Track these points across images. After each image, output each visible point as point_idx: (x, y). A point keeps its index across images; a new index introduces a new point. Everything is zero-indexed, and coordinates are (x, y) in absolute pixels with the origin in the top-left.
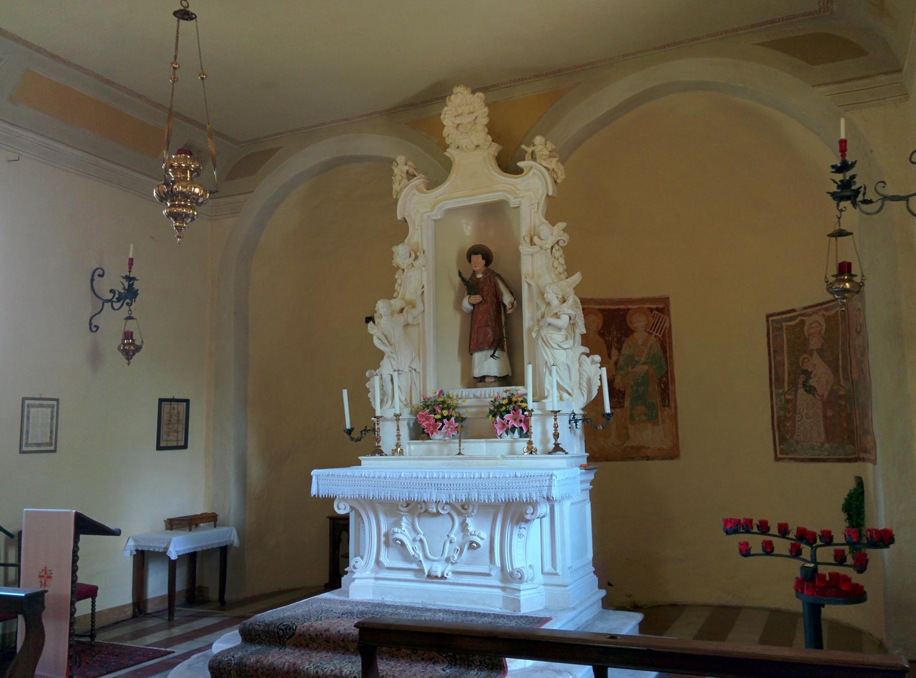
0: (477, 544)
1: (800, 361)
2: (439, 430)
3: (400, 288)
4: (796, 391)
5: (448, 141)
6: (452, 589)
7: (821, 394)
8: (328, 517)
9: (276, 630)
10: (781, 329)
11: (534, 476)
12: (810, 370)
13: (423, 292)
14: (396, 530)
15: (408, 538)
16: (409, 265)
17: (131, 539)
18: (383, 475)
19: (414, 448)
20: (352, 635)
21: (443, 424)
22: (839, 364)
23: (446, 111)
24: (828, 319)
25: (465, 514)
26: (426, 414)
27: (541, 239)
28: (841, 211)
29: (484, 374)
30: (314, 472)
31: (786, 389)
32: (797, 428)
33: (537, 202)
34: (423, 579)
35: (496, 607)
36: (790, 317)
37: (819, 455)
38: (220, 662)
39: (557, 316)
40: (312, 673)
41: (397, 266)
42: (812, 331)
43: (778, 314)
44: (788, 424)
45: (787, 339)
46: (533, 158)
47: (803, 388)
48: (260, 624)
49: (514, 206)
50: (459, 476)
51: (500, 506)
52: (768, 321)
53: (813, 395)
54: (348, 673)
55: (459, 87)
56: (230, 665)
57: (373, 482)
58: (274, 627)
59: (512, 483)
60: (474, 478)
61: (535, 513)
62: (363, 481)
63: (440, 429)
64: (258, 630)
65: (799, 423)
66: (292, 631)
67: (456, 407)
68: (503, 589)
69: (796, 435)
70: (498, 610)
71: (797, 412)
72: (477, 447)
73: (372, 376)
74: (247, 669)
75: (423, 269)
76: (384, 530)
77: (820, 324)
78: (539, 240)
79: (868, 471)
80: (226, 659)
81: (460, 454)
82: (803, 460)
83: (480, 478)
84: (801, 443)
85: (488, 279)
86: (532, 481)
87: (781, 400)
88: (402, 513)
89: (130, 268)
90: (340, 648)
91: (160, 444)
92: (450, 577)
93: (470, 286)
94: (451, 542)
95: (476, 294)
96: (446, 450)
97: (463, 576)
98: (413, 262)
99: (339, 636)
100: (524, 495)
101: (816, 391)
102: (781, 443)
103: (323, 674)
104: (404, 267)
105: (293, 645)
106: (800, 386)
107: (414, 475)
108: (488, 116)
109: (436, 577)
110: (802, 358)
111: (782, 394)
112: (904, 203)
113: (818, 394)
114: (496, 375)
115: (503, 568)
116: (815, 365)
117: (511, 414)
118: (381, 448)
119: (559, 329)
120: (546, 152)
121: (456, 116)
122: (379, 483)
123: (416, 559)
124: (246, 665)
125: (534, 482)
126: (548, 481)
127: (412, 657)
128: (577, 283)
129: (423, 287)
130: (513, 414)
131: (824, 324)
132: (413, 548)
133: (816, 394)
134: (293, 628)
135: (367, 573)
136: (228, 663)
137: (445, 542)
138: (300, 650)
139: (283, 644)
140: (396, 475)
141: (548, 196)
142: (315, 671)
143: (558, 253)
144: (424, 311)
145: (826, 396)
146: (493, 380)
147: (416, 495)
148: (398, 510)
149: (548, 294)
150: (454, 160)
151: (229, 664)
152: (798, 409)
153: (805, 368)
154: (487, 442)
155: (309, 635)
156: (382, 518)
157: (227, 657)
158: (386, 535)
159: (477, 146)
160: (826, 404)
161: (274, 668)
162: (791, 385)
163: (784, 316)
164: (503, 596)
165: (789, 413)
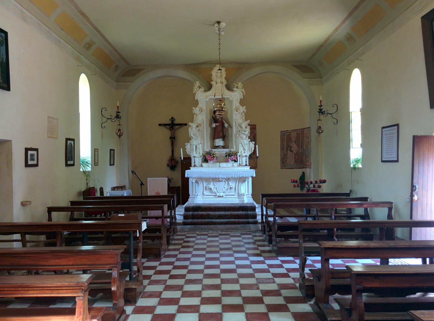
0: (232, 188)
4: (288, 151)
5: (213, 79)
12: (292, 146)
14: (209, 185)
17: (108, 193)
18: (208, 171)
19: (204, 165)
21: (213, 159)
24: (297, 134)
28: (320, 115)
30: (186, 171)
31: (285, 150)
36: (287, 132)
39: (245, 131)
46: (237, 88)
52: (281, 133)
63: (213, 160)
67: (216, 154)
68: (238, 198)
72: (223, 165)
73: (187, 145)
74: (195, 216)
76: (205, 186)
79: (307, 171)
81: (220, 166)
87: (283, 153)
89: (118, 109)
91: (395, 161)
92: (224, 196)
93: (215, 120)
94: (225, 188)
96: (214, 166)
102: (283, 164)
104: (197, 114)
106: (289, 150)
107: (217, 171)
109: (221, 197)
112: (331, 115)
114: (223, 145)
115: (238, 193)
116: (293, 145)
119: (245, 134)
120: (241, 87)
129: (203, 120)
131: (296, 135)
135: (200, 197)
141: (241, 98)
143: (244, 114)
144: (204, 127)
148: (210, 180)
150: (213, 84)
153: (290, 145)
154: (226, 163)
156: (204, 183)
158: (206, 187)
163: (286, 132)
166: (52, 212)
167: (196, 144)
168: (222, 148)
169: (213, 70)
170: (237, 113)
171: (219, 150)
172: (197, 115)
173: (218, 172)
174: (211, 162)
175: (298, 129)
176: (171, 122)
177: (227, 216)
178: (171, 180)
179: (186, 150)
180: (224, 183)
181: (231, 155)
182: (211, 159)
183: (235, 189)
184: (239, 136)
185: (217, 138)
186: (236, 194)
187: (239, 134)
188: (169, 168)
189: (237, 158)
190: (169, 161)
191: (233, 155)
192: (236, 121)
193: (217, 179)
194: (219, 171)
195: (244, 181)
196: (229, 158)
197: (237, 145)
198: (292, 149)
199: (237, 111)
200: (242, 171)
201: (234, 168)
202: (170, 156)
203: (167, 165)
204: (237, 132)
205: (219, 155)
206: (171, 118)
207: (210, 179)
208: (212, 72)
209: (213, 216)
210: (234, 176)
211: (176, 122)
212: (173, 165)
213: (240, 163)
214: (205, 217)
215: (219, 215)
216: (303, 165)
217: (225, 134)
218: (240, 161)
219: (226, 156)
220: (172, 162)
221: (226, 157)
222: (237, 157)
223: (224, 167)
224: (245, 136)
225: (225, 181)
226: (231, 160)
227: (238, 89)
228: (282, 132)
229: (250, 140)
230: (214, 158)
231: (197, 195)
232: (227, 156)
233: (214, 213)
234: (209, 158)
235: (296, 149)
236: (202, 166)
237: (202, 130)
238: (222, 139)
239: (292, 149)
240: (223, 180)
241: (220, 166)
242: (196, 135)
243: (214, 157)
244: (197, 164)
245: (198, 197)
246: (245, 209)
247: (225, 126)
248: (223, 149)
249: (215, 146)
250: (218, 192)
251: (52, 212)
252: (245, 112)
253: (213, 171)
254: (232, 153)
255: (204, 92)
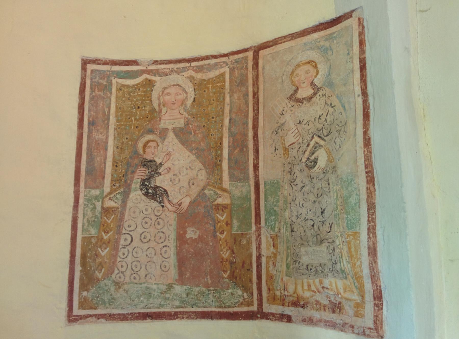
1: (140, 145)
4: (126, 195)
7: (175, 201)
10: (107, 88)
12: (158, 161)
22: (221, 155)
31: (107, 189)
32: (119, 259)
37: (161, 306)
42: (167, 98)
44: (104, 252)
52: (84, 69)
65: (125, 251)
69: (116, 271)
71: (124, 231)
77: (184, 91)
82: (124, 318)
84: (126, 287)
87: (95, 208)
102: (83, 287)
106: (136, 184)
111: (96, 198)
116: (169, 154)
145: (185, 205)
152: (126, 225)
153: (149, 157)
162: (117, 185)
166: (264, 311)
175: (207, 58)
198: (158, 181)
216: (246, 289)
235: (191, 183)
239: (158, 181)
251: (264, 311)
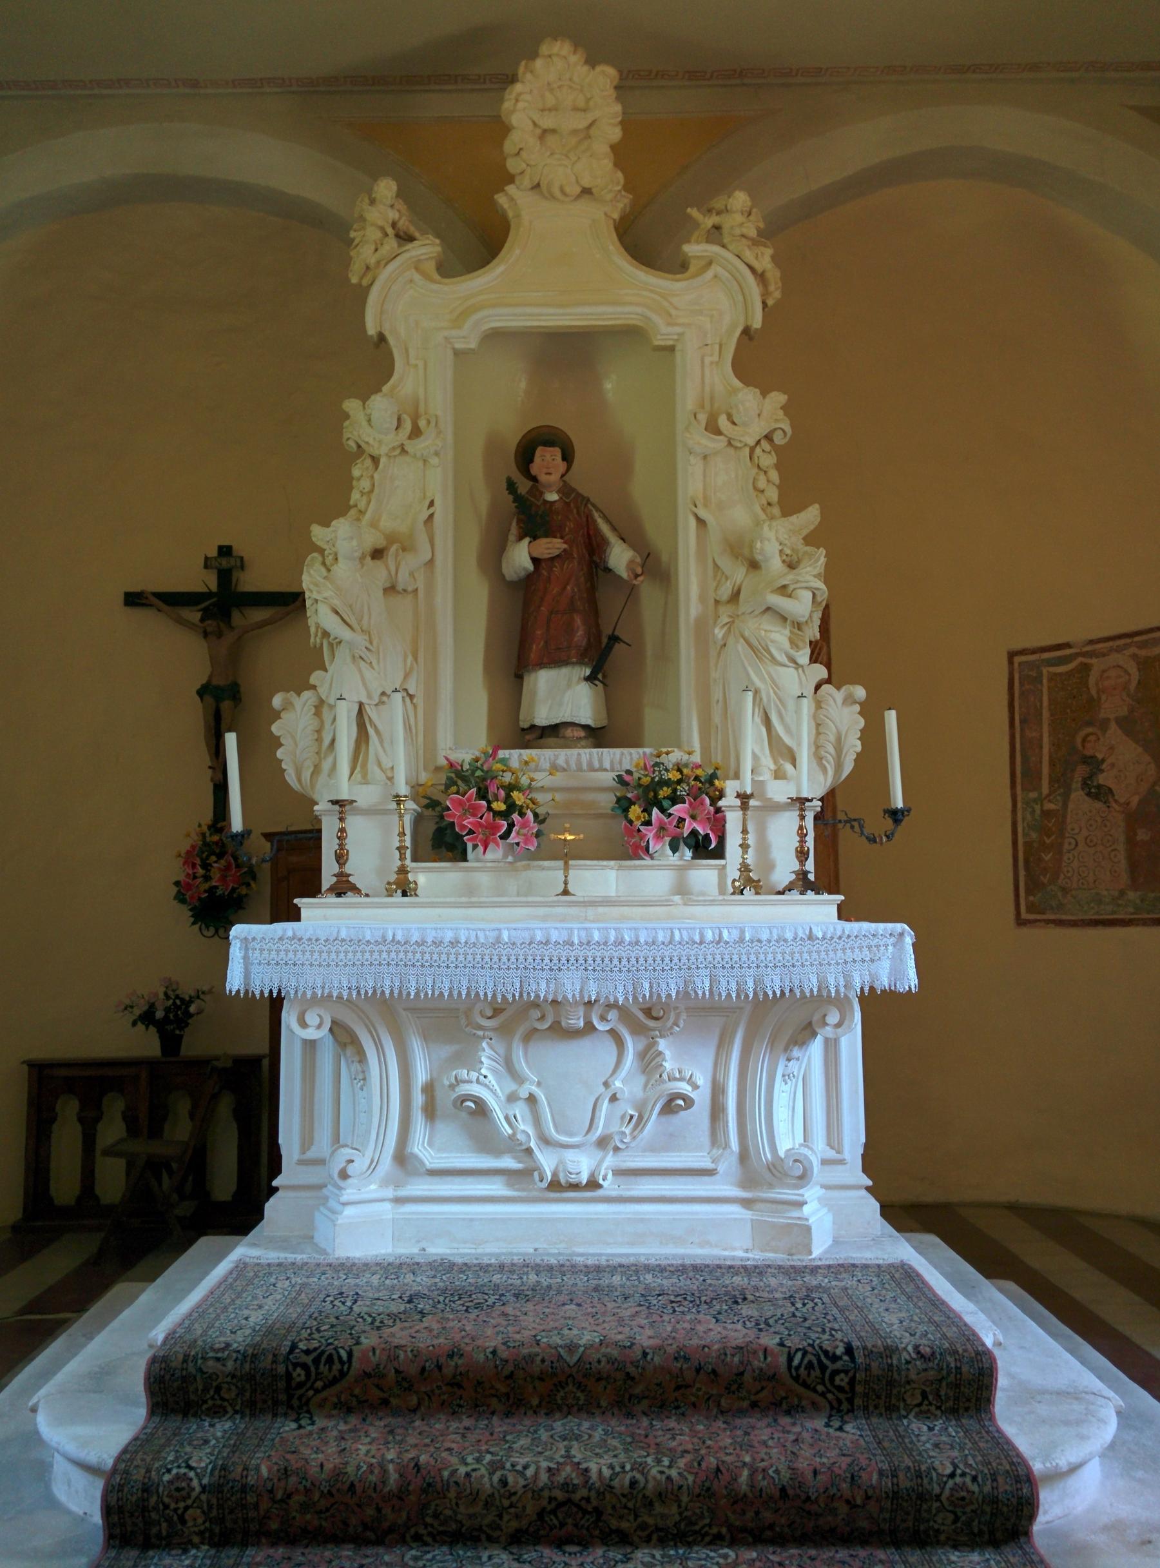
0: (684, 1098)
1: (1079, 740)
2: (501, 837)
3: (369, 502)
5: (512, 165)
6: (619, 1213)
7: (1122, 800)
8: (24, 1062)
9: (281, 1369)
11: (856, 937)
12: (1100, 756)
13: (431, 516)
14: (463, 1073)
15: (495, 1094)
16: (394, 449)
18: (449, 936)
20: (539, 1359)
21: (511, 826)
23: (519, 94)
25: (653, 1030)
26: (469, 800)
27: (734, 423)
29: (564, 720)
31: (1045, 790)
32: (1064, 864)
33: (718, 341)
34: (535, 1194)
35: (734, 1249)
36: (1059, 658)
37: (1114, 912)
38: (146, 1489)
39: (783, 590)
40: (488, 1486)
41: (359, 446)
43: (1034, 651)
44: (1047, 857)
45: (1050, 700)
46: (715, 234)
47: (1083, 789)
48: (220, 1355)
49: (662, 343)
50: (660, 939)
51: (741, 1008)
53: (1105, 803)
54: (607, 1472)
55: (559, 43)
56: (184, 1493)
57: (418, 956)
58: (274, 1362)
59: (801, 953)
60: (701, 943)
61: (846, 1022)
62: (389, 952)
63: (505, 837)
64: (213, 1376)
65: (1071, 856)
66: (337, 1366)
68: (747, 1203)
69: (1062, 876)
70: (740, 1254)
71: (1067, 835)
73: (288, 706)
74: (251, 1499)
75: (434, 461)
76: (421, 1075)
77: (1126, 671)
78: (729, 424)
80: (167, 1478)
81: (566, 892)
82: (1074, 924)
83: (718, 942)
84: (1074, 892)
85: (572, 505)
86: (852, 949)
87: (1033, 812)
88: (481, 1033)
90: (494, 1401)
92: (609, 1185)
94: (614, 1098)
95: (548, 534)
97: (639, 1179)
98: (406, 442)
99: (496, 1367)
100: (832, 981)
101: (1113, 795)
102: (1029, 892)
103: (524, 1487)
104: (383, 450)
105: (335, 1406)
106: (1076, 784)
107: (539, 936)
108: (621, 123)
109: (575, 1187)
110: (1082, 733)
111: (1035, 801)
113: (1116, 801)
114: (589, 722)
116: (1112, 748)
117: (686, 805)
118: (351, 879)
121: (542, 110)
122: (435, 957)
123: (521, 1144)
124: (244, 1489)
125: (857, 950)
126: (890, 948)
127: (723, 1402)
128: (812, 527)
129: (432, 504)
130: (691, 804)
132: (507, 1118)
133: (1111, 800)
134: (340, 1357)
135: (373, 1189)
136: (178, 1490)
137: (597, 1100)
138: (376, 1414)
139: (300, 1407)
140: (486, 937)
142: (496, 1478)
143: (768, 460)
144: (431, 562)
146: (582, 734)
147: (543, 986)
149: (766, 542)
150: (518, 216)
151: (180, 1490)
152: (1069, 827)
153: (1088, 753)
154: (620, 868)
155: (397, 1371)
156: (418, 1050)
157: (169, 1471)
159: (586, 192)
160: (1133, 819)
161: (352, 1485)
162: (1056, 785)
163: (1046, 655)
164: (752, 1220)
165: (1049, 837)
167: (364, 700)
168: (583, 743)
169: (518, 87)
170: (711, 445)
171: (562, 756)
172: (375, 460)
173: (547, 942)
174: (489, 855)
176: (211, 582)
177: (658, 1508)
178: (192, 1009)
179: (280, 754)
180: (608, 1050)
181: (665, 792)
182: (494, 828)
183: (717, 1111)
184: (731, 641)
185: (541, 665)
186: (728, 1164)
187: (734, 618)
188: (184, 914)
189: (718, 821)
190: (188, 859)
191: (682, 790)
192: (702, 513)
193: (536, 1014)
194: (564, 936)
195: (806, 1033)
196: (648, 823)
197: (717, 718)
198: (1101, 779)
199: (718, 432)
200: (782, 940)
201: (698, 910)
202: (200, 826)
203: (175, 889)
204: (717, 602)
205: (558, 797)
206: (214, 553)
207: (468, 1012)
208: (507, 105)
209: (478, 1509)
210: (703, 984)
211: (251, 581)
212: (219, 892)
213: (745, 868)
214: (379, 1510)
215: (559, 1495)
217: (607, 631)
218: (744, 847)
219: (624, 805)
220: (206, 866)
221: (626, 810)
222: (718, 810)
223: (607, 902)
224: (787, 632)
225: (612, 1032)
226: (668, 839)
227: (724, 246)
228: (1023, 658)
229: (821, 672)
230: (515, 817)
231: (344, 1175)
232: (631, 803)
233: (495, 1467)
234: (468, 822)
236: (405, 888)
237: (421, 585)
238: (588, 672)
239: (1101, 779)
240: (601, 1027)
241: (570, 888)
242: (360, 621)
243: (512, 807)
244: (361, 868)
245: (349, 1194)
246: (859, 1389)
247: (608, 570)
248: (595, 750)
249: (526, 726)
250: (545, 1141)
252: (778, 439)
253: (505, 936)
254: (674, 776)
255: (437, 277)
